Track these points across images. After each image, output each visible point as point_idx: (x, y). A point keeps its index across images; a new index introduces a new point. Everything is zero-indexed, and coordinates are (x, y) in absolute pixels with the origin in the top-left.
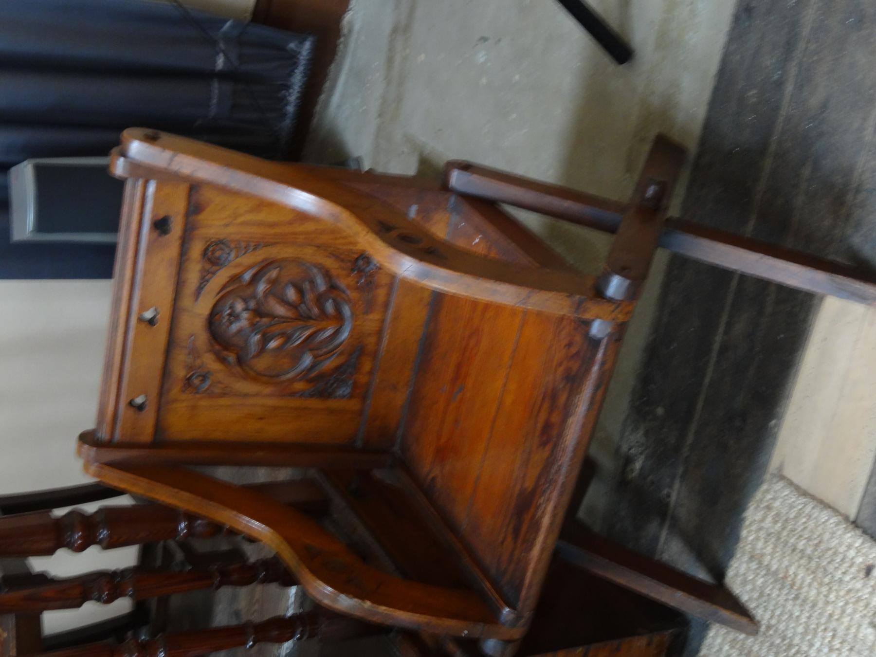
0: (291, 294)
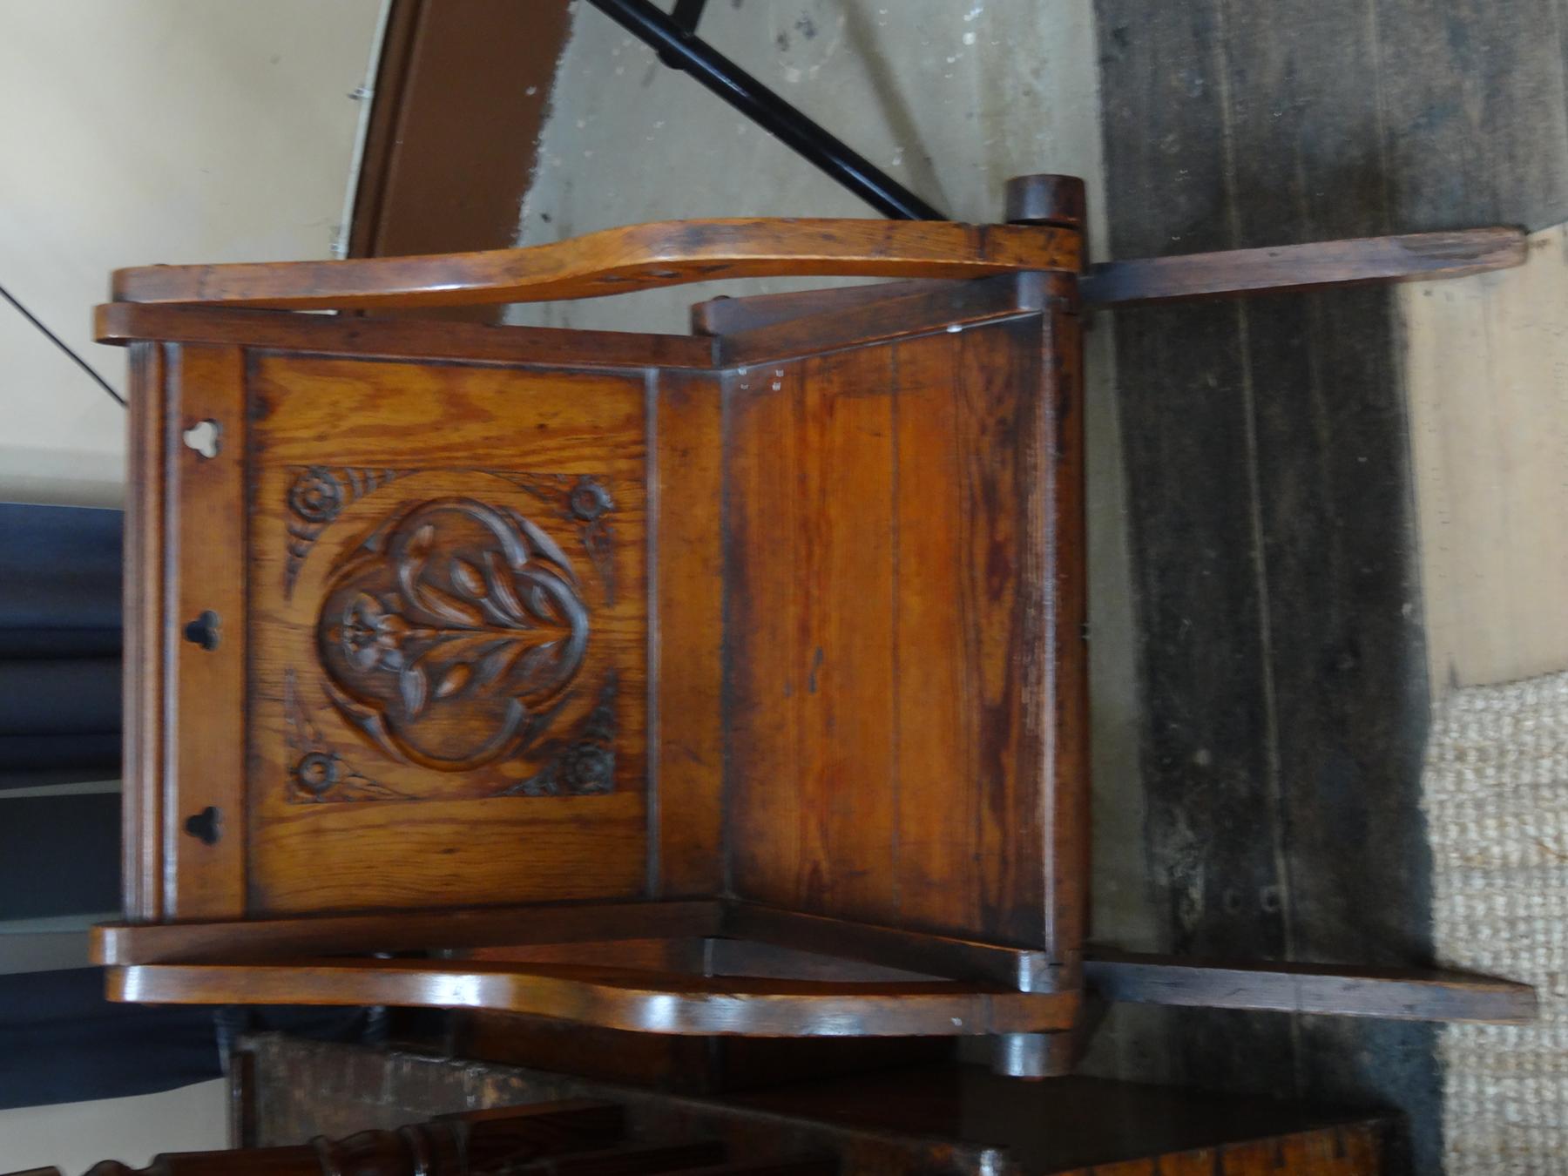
0: (465, 578)
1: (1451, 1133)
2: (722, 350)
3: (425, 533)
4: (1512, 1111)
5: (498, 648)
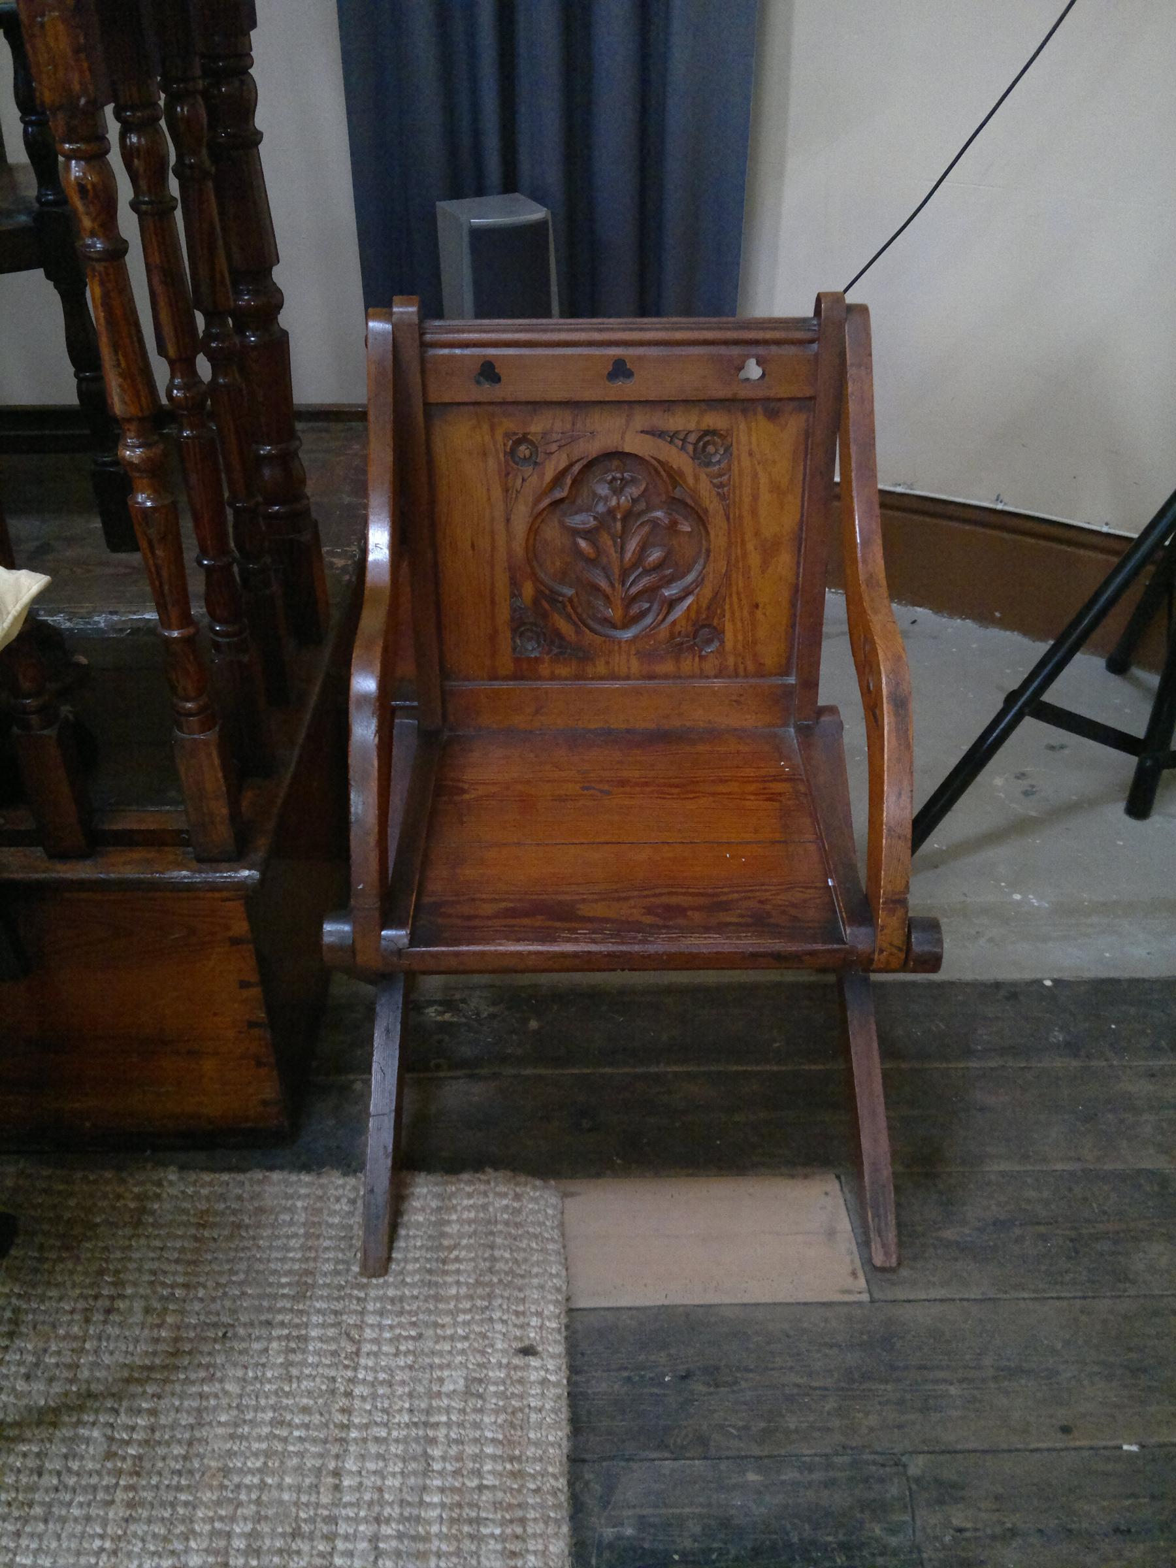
0: (655, 555)
1: (276, 1176)
2: (808, 726)
3: (686, 528)
4: (286, 1217)
5: (608, 577)
